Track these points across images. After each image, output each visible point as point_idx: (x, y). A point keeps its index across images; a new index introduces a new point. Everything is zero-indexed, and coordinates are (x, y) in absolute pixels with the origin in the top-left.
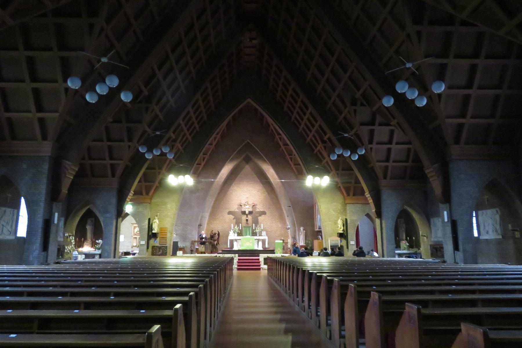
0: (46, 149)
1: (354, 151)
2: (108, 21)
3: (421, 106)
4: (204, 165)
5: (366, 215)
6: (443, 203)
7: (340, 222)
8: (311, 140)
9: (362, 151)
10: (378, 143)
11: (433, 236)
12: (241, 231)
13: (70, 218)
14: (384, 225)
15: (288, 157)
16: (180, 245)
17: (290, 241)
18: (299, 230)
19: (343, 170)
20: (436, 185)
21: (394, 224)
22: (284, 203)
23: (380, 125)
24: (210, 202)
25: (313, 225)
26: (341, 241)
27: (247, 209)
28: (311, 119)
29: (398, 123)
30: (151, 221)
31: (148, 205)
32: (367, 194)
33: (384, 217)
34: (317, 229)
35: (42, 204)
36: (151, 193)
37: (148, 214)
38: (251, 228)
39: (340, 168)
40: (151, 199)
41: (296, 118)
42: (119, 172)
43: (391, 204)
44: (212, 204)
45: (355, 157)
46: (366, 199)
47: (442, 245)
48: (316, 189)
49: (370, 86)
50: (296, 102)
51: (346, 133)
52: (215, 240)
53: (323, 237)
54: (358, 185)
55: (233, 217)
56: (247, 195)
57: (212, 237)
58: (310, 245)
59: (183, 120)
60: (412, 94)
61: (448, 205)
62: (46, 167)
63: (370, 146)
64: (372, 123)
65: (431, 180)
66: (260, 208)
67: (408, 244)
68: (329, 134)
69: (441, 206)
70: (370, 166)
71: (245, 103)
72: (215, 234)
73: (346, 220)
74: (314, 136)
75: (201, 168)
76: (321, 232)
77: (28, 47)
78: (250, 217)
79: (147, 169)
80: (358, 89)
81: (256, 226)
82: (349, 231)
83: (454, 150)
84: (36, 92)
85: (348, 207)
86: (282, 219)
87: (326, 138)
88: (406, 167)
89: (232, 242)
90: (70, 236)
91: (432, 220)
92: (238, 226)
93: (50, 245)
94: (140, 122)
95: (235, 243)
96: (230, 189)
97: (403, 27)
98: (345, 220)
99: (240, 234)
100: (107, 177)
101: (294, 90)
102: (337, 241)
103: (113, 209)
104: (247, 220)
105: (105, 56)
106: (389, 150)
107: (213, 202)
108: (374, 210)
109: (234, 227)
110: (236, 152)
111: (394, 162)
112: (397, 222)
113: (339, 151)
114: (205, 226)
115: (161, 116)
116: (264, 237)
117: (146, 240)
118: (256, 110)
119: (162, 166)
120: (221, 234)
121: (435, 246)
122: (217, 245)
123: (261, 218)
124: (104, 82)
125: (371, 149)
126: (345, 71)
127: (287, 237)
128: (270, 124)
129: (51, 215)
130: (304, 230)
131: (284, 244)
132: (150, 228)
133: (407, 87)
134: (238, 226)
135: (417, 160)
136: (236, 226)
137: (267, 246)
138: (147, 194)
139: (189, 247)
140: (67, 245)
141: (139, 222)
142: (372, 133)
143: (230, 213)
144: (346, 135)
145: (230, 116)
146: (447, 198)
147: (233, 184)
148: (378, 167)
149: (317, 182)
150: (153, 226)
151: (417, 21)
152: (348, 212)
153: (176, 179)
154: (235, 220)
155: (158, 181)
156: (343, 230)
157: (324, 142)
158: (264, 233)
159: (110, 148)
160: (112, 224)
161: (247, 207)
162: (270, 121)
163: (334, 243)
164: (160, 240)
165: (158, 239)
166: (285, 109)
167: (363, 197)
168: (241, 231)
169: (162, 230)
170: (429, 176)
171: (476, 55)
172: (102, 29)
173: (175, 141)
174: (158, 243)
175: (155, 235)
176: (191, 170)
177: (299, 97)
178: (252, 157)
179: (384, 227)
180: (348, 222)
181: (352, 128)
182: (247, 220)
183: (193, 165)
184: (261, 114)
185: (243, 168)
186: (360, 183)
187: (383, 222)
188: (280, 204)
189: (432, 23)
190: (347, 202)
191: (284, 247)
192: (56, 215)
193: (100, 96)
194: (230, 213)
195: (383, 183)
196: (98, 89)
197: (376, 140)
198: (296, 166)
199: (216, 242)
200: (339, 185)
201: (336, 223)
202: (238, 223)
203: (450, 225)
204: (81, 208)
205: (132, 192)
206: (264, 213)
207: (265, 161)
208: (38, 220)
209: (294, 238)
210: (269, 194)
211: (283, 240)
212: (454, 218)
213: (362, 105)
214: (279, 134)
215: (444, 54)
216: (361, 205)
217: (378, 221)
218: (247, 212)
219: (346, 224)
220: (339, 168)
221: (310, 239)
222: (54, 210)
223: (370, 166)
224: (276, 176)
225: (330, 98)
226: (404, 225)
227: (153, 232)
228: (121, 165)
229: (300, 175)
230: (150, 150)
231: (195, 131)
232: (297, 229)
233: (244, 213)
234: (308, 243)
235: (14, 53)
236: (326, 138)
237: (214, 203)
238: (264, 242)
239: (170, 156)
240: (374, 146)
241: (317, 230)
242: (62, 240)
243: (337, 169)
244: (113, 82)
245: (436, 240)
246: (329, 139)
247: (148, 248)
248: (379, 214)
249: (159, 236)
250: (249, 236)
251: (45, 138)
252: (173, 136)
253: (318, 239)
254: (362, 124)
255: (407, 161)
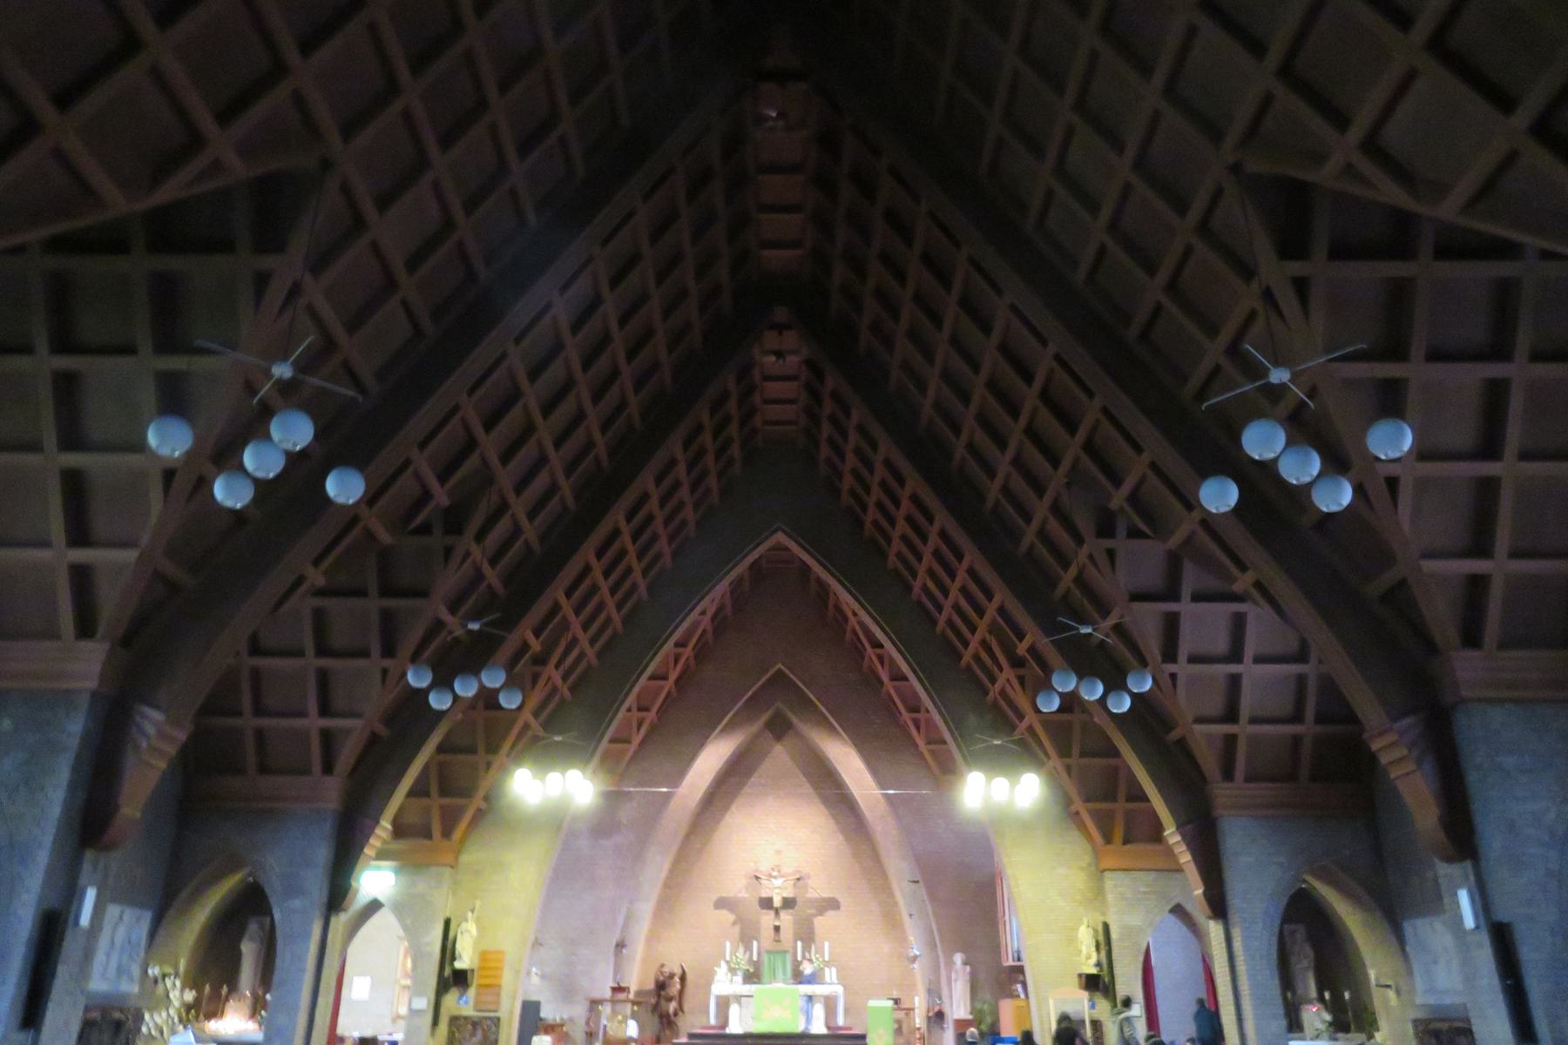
0: (87, 665)
1: (1115, 683)
2: (318, 263)
3: (1334, 508)
4: (643, 743)
5: (1171, 911)
6: (1450, 859)
7: (1086, 938)
8: (976, 657)
9: (1144, 681)
10: (1194, 659)
11: (1420, 985)
12: (757, 965)
13: (171, 912)
14: (1238, 945)
15: (906, 716)
16: (548, 1013)
17: (919, 1003)
18: (950, 964)
19: (1083, 754)
20: (1414, 789)
21: (1275, 939)
22: (898, 868)
23: (1197, 597)
24: (657, 866)
25: (995, 947)
26: (1093, 1006)
27: (778, 890)
28: (973, 587)
29: (1258, 585)
30: (453, 926)
31: (447, 871)
32: (1172, 835)
33: (1234, 917)
34: (1010, 962)
35: (42, 857)
36: (457, 834)
37: (443, 902)
38: (789, 958)
39: (1076, 750)
40: (458, 853)
41: (925, 588)
42: (347, 756)
43: (1259, 869)
44: (663, 875)
45: (1120, 705)
46: (1169, 853)
47: (1468, 1020)
48: (1001, 820)
49: (1153, 466)
50: (924, 538)
51: (1084, 622)
52: (670, 999)
53: (1030, 989)
54: (1142, 805)
55: (732, 917)
56: (776, 843)
57: (661, 986)
58: (989, 1020)
59: (568, 595)
60: (1301, 468)
61: (1468, 864)
62: (74, 728)
63: (1171, 668)
64: (1172, 594)
65: (1392, 776)
66: (818, 888)
67: (1328, 1017)
68: (1033, 635)
69: (1444, 869)
70: (1174, 735)
71: (768, 544)
72: (672, 976)
73: (1106, 927)
74: (984, 644)
75: (630, 754)
76: (1020, 970)
77: (64, 343)
78: (786, 919)
79: (441, 749)
80: (1117, 482)
81: (807, 948)
82: (1118, 971)
83: (1467, 669)
84: (74, 484)
85: (1110, 881)
86: (891, 920)
87: (1022, 649)
88: (1296, 741)
89: (724, 1004)
90: (164, 976)
91: (1408, 927)
92: (748, 948)
93: (50, 1005)
94: (422, 593)
95: (734, 1010)
96: (723, 823)
97: (1247, 272)
98: (1100, 928)
99: (752, 977)
100: (305, 771)
101: (915, 499)
102: (1080, 1004)
103: (316, 883)
104: (777, 929)
105: (475, 618)
106: (1235, 682)
107: (667, 866)
108: (1199, 891)
109: (734, 953)
110: (740, 704)
111: (1254, 720)
112: (1281, 933)
113: (1065, 682)
114: (638, 950)
115: (492, 576)
116: (831, 986)
117: (432, 996)
118: (806, 569)
119: (484, 739)
120: (689, 977)
121: (1432, 1026)
122: (676, 1014)
123: (822, 923)
124: (267, 436)
125: (1173, 676)
126: (1071, 428)
127: (912, 988)
128: (850, 614)
129: (72, 895)
130: (965, 964)
131: (901, 1015)
132: (448, 951)
133: (1281, 438)
134: (748, 948)
135: (1336, 710)
136: (741, 950)
137: (841, 1021)
138: (447, 833)
139: (582, 1022)
140: (151, 1010)
141: (413, 932)
142: (1171, 625)
143: (722, 903)
144: (1086, 630)
145: (722, 588)
146: (1462, 840)
147: (733, 808)
148: (1203, 738)
149: (1002, 794)
150: (458, 946)
151: (1292, 246)
152: (1110, 897)
153: (537, 782)
154: (737, 929)
155: (481, 793)
156: (1098, 964)
157: (1017, 663)
158: (831, 974)
159: (323, 679)
160: (307, 935)
161: (778, 882)
162: (846, 599)
163: (1070, 1009)
164: (478, 994)
165: (472, 992)
166: (892, 561)
167: (1158, 847)
168: (757, 965)
169: (489, 959)
170: (1384, 759)
171: (1498, 351)
172: (295, 291)
173: (540, 660)
174: (471, 1003)
175: (460, 979)
176: (592, 755)
177: (931, 519)
178: (795, 720)
179: (1240, 957)
180: (1114, 936)
181: (1105, 612)
182: (777, 929)
183: (599, 741)
184: (821, 583)
185: (762, 756)
186: (1144, 798)
187: (1236, 933)
188: (883, 874)
189: (1341, 251)
190: (1105, 865)
191: (899, 1022)
192: (91, 895)
193: (258, 483)
194: (722, 903)
195: (1222, 793)
196: (249, 459)
197: (1185, 648)
198: (933, 747)
199: (672, 1006)
200: (1073, 808)
201: (1072, 939)
202: (746, 937)
203: (1485, 939)
204: (216, 878)
205: (386, 824)
206: (832, 904)
207: (832, 729)
208: (20, 912)
209: (934, 992)
210: (848, 839)
211: (896, 1001)
212: (1502, 914)
213: (1134, 533)
214: (877, 645)
215: (1395, 351)
216: (1153, 875)
217: (1215, 930)
218: (777, 902)
219: (1105, 941)
220: (1075, 747)
221: (988, 997)
222: (82, 881)
223: (1174, 735)
224: (868, 778)
225: (1028, 518)
226: (1309, 951)
227: (458, 965)
228: (354, 731)
229: (945, 771)
230: (443, 681)
231: (609, 632)
232: (942, 960)
233: (767, 903)
234: (981, 1011)
235: (298, 723)
236: (1022, 649)
237: (671, 871)
238: (830, 1004)
239: (510, 701)
240: (1182, 668)
241: (1010, 963)
242: (135, 989)
243: (1064, 752)
244: (294, 432)
245: (1431, 1001)
246: (1032, 650)
247: (435, 1022)
248: (1218, 907)
249: (475, 981)
250: (780, 985)
251: (86, 629)
252: (536, 645)
253: (1013, 995)
254: (1138, 597)
255: (1297, 718)
